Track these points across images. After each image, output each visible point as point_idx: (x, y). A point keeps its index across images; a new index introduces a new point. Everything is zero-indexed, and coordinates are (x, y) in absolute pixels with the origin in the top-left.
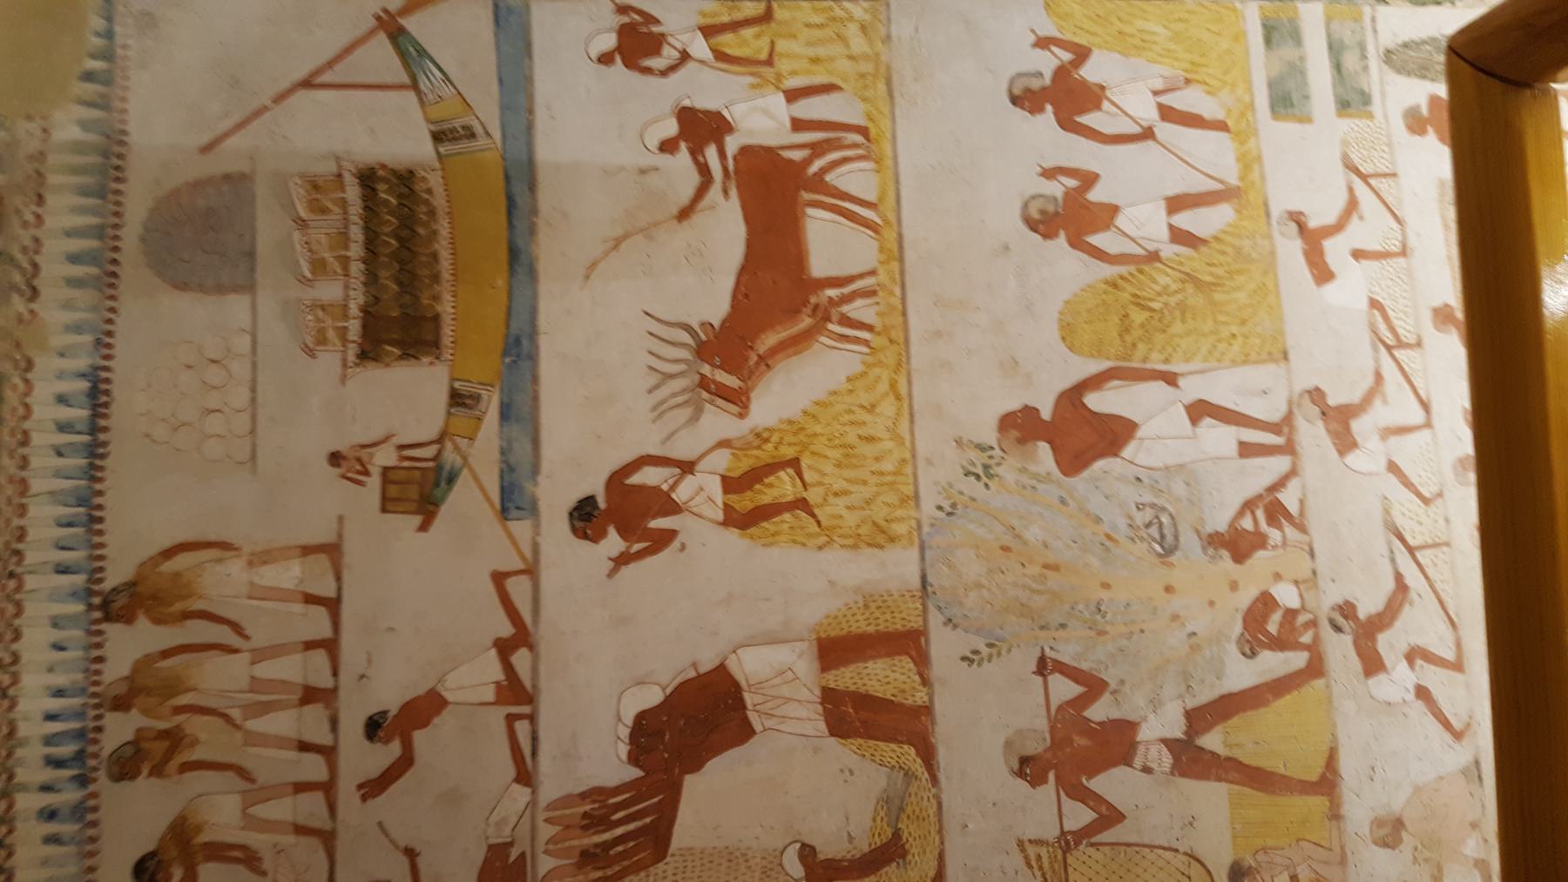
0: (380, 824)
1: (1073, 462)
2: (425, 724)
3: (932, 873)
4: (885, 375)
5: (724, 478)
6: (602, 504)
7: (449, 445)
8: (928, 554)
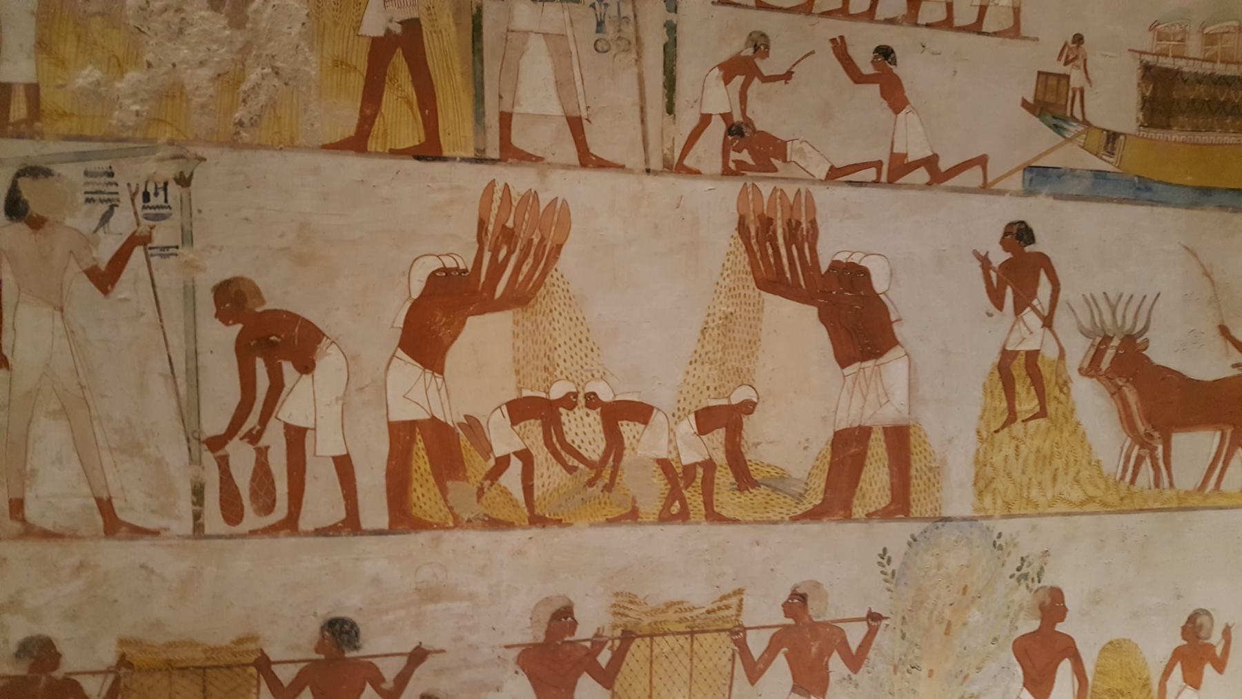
0: (813, 52)
1: (1025, 649)
2: (884, 95)
3: (724, 513)
4: (1098, 493)
5: (1037, 352)
6: (1028, 249)
7: (1081, 129)
8: (966, 524)
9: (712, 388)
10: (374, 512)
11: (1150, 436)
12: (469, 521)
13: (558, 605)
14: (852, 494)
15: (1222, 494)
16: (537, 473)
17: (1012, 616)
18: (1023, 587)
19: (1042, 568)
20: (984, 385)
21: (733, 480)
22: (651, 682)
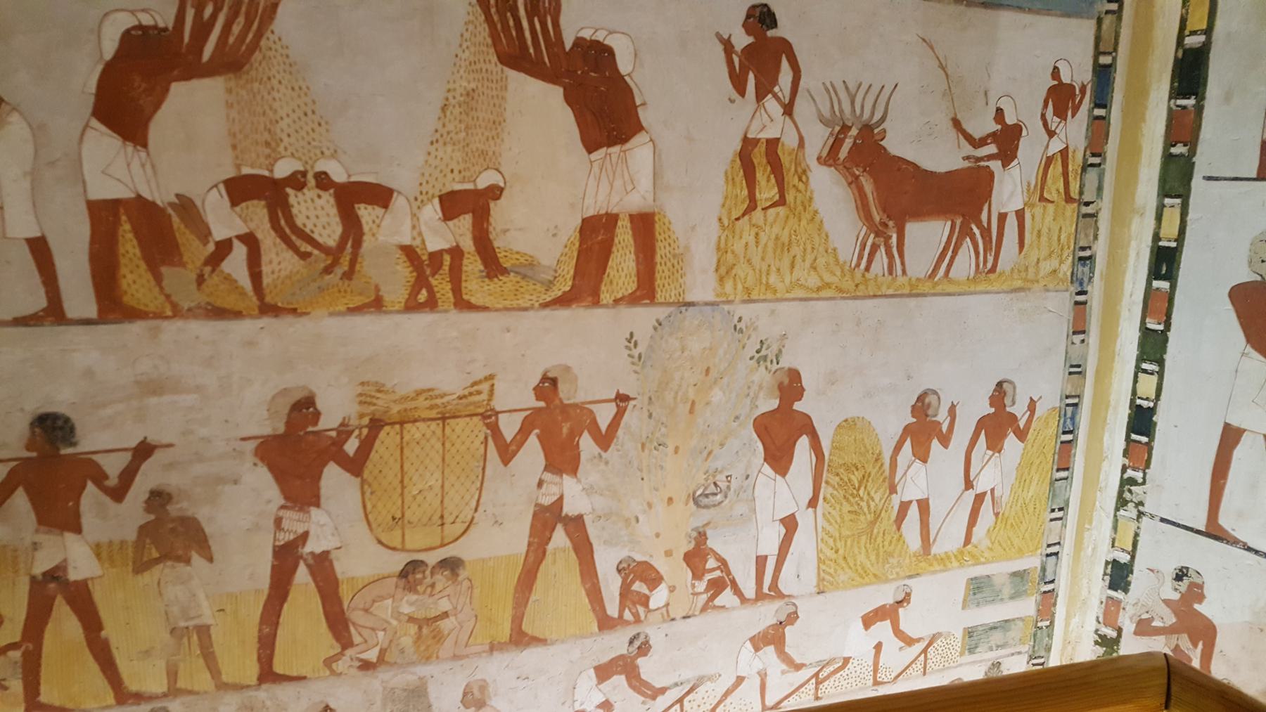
1: (763, 426)
3: (473, 300)
4: (834, 280)
5: (778, 140)
6: (770, 33)
9: (456, 172)
10: (79, 297)
11: (886, 225)
12: (190, 310)
13: (298, 396)
14: (601, 280)
15: (951, 281)
16: (265, 259)
17: (752, 394)
18: (762, 368)
19: (780, 351)
20: (726, 173)
21: (482, 268)
22: (402, 467)
